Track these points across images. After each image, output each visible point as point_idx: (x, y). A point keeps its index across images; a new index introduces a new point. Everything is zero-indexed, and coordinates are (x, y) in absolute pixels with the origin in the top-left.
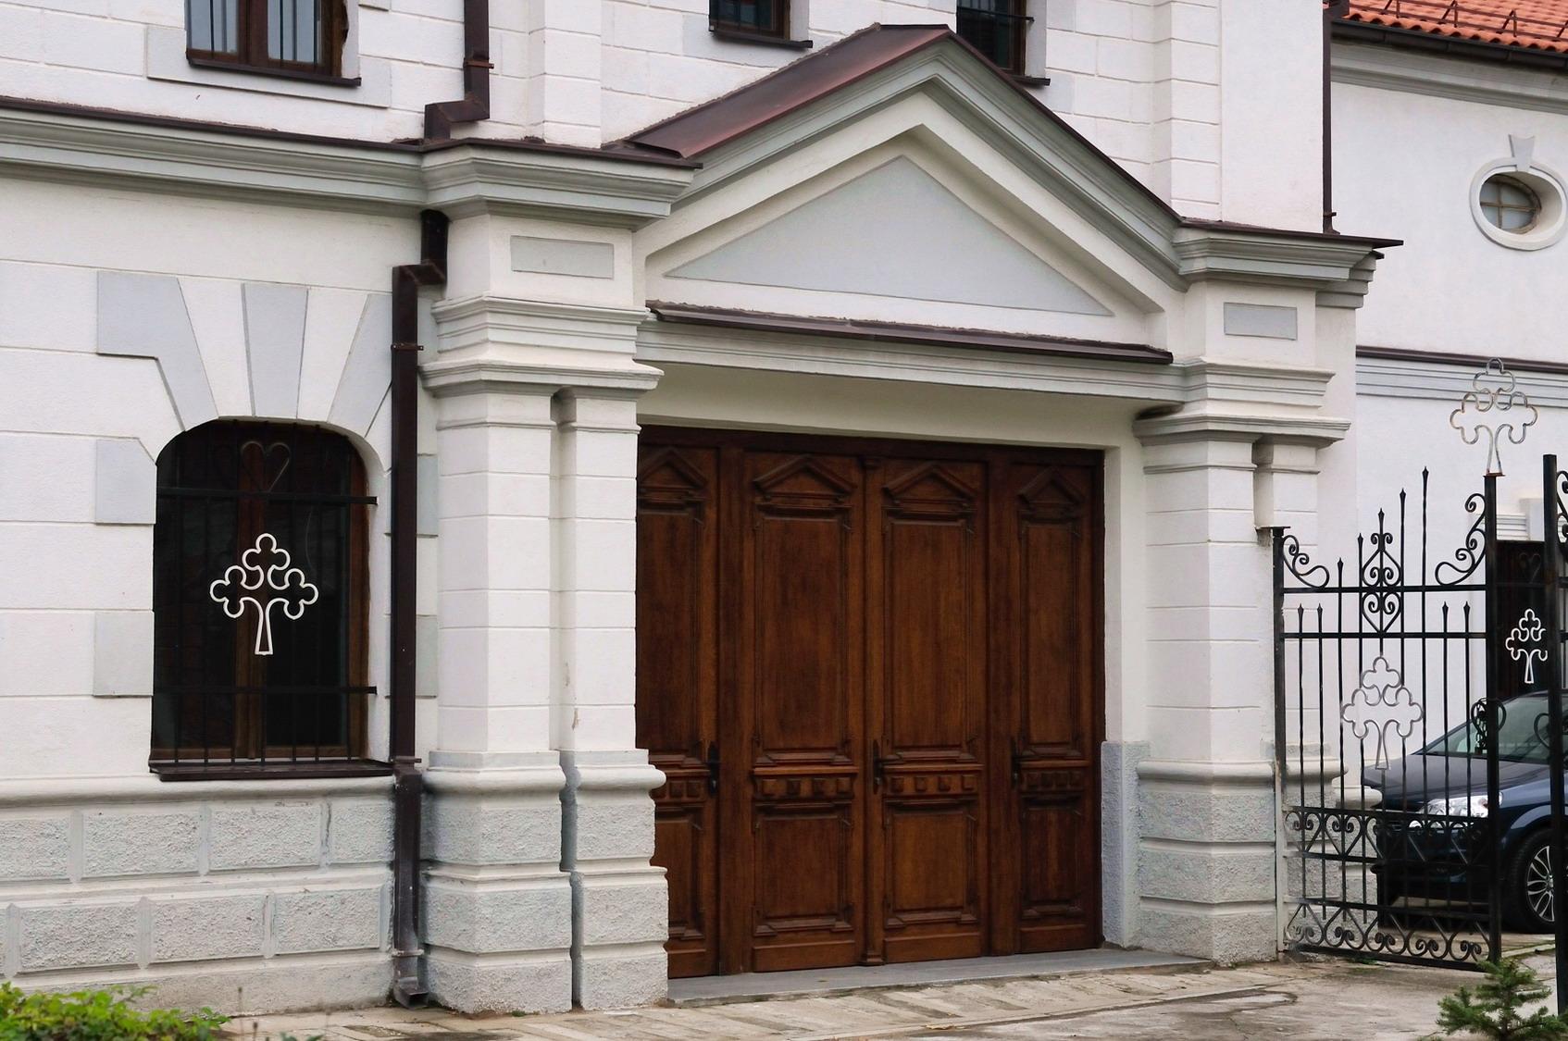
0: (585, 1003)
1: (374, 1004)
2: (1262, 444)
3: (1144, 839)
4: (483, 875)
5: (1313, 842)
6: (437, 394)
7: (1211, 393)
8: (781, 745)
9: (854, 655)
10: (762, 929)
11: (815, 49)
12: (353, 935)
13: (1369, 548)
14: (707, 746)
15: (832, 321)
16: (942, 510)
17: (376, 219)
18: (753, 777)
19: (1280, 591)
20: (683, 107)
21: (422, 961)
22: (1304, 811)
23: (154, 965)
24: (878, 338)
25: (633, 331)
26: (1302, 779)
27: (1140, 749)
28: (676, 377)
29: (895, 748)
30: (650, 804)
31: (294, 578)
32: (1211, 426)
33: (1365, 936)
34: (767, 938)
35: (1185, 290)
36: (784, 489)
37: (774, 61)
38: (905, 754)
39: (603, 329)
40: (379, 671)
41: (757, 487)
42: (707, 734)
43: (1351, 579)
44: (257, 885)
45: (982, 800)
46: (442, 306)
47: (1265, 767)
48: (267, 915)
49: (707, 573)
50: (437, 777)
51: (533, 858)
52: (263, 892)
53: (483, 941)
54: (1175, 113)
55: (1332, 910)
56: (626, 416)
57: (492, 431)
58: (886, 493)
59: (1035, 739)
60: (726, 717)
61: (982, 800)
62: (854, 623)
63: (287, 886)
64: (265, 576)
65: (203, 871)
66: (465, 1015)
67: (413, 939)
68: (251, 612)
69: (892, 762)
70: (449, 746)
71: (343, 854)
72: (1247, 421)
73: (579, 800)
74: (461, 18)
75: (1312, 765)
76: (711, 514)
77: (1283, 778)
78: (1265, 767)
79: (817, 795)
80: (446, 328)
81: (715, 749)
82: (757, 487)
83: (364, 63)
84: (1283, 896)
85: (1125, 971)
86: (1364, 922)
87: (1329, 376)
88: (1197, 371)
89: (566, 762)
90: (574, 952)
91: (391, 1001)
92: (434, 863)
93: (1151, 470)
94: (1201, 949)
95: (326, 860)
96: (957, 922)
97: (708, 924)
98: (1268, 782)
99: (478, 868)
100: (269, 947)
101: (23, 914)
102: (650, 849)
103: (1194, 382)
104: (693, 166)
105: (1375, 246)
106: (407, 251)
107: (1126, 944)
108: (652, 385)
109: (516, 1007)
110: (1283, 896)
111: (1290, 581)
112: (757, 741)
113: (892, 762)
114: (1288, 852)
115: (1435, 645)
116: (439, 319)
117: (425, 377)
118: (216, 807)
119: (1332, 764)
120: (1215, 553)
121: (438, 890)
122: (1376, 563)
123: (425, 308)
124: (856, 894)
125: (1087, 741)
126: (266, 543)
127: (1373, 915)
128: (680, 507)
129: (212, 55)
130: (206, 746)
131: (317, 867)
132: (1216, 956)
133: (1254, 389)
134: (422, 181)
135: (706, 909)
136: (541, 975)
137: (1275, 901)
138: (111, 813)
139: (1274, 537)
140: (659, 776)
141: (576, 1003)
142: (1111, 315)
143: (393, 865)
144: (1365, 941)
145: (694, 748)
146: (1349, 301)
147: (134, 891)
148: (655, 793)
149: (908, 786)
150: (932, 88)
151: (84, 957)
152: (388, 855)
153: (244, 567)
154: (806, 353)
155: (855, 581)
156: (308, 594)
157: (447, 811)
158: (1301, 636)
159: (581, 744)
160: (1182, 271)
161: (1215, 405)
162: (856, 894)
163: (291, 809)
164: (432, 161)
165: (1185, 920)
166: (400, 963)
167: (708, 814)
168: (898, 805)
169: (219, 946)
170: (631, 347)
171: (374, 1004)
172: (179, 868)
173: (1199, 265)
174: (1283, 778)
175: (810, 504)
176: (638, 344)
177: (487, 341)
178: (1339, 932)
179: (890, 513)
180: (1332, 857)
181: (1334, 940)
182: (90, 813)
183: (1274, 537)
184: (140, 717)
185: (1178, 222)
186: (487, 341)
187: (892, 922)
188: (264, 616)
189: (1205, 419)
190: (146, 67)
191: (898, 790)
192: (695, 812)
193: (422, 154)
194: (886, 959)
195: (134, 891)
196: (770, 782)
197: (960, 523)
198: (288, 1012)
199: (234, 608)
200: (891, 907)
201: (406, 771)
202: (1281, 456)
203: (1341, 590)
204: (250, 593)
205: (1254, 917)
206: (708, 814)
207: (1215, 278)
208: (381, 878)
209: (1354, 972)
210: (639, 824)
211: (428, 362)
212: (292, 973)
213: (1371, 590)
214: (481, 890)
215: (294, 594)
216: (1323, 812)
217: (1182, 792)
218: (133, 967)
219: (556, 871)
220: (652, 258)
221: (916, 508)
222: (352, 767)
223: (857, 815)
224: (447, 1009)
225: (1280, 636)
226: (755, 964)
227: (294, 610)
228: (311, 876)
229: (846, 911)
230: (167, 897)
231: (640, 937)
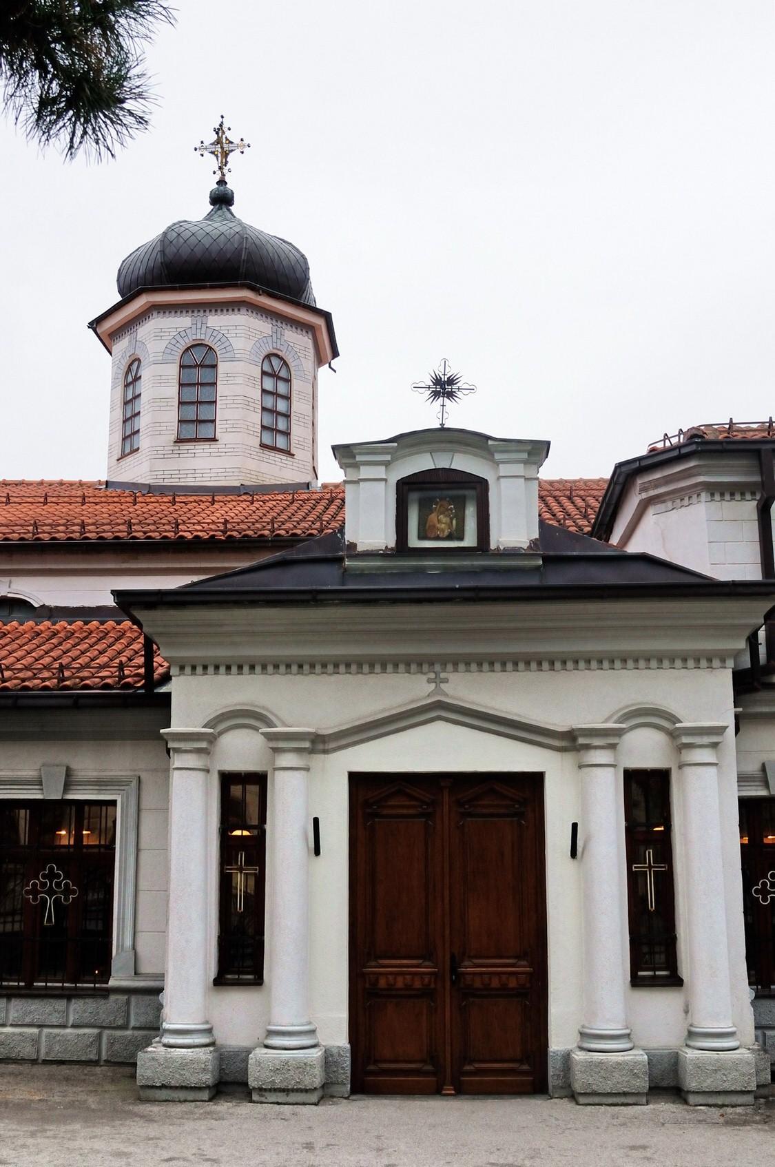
215: (67, 891)
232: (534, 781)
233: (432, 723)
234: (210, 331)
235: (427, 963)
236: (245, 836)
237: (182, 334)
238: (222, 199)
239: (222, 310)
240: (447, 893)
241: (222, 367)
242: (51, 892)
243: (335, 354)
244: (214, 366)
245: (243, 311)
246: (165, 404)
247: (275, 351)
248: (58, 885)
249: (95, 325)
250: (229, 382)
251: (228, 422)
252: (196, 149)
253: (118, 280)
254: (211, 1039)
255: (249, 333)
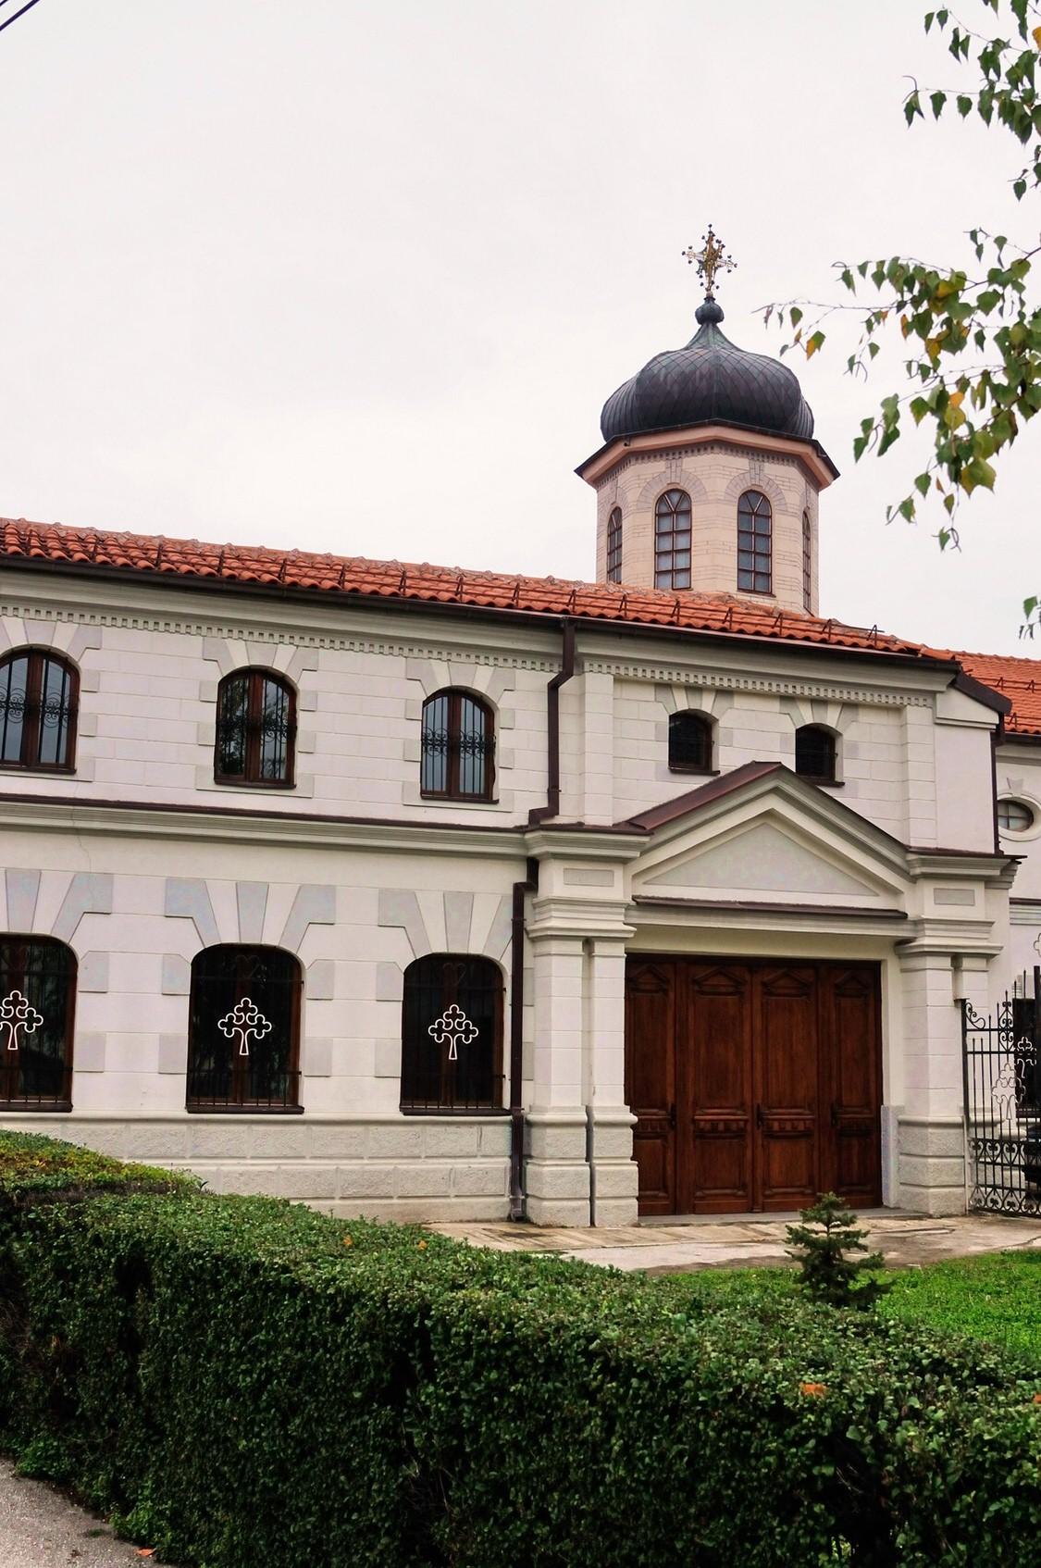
0: (596, 1224)
1: (501, 1220)
2: (957, 958)
3: (901, 1154)
4: (548, 1162)
5: (981, 1156)
6: (534, 940)
7: (927, 933)
8: (709, 1105)
9: (747, 1065)
10: (699, 1194)
11: (722, 774)
12: (492, 1188)
13: (1002, 1009)
14: (670, 1105)
15: (729, 902)
16: (793, 992)
17: (507, 862)
18: (694, 1121)
19: (965, 1031)
20: (657, 804)
21: (524, 1202)
22: (976, 1140)
23: (400, 1197)
24: (749, 910)
25: (623, 910)
26: (976, 1125)
27: (900, 1109)
28: (642, 930)
29: (769, 1108)
30: (631, 1131)
31: (260, 1019)
32: (926, 949)
33: (1021, 1204)
34: (702, 1198)
35: (915, 883)
36: (710, 982)
37: (705, 780)
38: (775, 1111)
39: (957, 927)
40: (507, 1070)
41: (695, 982)
42: (670, 1099)
43: (995, 1026)
44: (446, 1163)
45: (816, 1134)
46: (535, 900)
47: (958, 1118)
48: (452, 1178)
49: (670, 1022)
50: (532, 1117)
51: (572, 1156)
52: (450, 1167)
53: (546, 1192)
54: (911, 796)
55: (989, 1190)
56: (620, 949)
57: (554, 957)
58: (764, 984)
59: (844, 1103)
60: (680, 1091)
61: (816, 1134)
62: (747, 1046)
63: (461, 1165)
64: (454, 1024)
65: (423, 1156)
66: (539, 1227)
67: (519, 1191)
68: (238, 1035)
69: (768, 1114)
70: (538, 1103)
71: (488, 1152)
72: (946, 946)
73: (595, 1129)
74: (547, 769)
75: (988, 1118)
76: (672, 995)
77: (968, 1124)
78: (958, 1118)
79: (727, 1129)
80: (537, 910)
81: (674, 1107)
82: (695, 982)
83: (501, 792)
84: (968, 1183)
85: (880, 1218)
86: (1018, 1197)
87: (993, 923)
88: (919, 923)
89: (588, 1111)
90: (592, 1199)
91: (509, 1219)
92: (530, 1157)
93: (904, 971)
94: (924, 1210)
95: (480, 1154)
96: (803, 1194)
97: (671, 1190)
98: (960, 1126)
99: (545, 1159)
100: (452, 1192)
101: (342, 1172)
102: (631, 1153)
103: (920, 927)
104: (650, 833)
105: (1015, 860)
106: (520, 876)
107: (892, 1206)
108: (632, 935)
109: (562, 1224)
110: (968, 1183)
111: (969, 1026)
112: (695, 1104)
113: (768, 1114)
114: (970, 1161)
115: (986, 1057)
116: (535, 906)
117: (528, 933)
118: (428, 1128)
119: (996, 1117)
120: (931, 1012)
121: (530, 1169)
122: (1005, 1017)
123: (528, 902)
124: (748, 1178)
125: (873, 1107)
126: (454, 1009)
127: (1023, 1194)
128: (656, 992)
129: (433, 792)
130: (214, 1096)
131: (475, 1157)
132: (931, 1212)
133: (969, 931)
134: (524, 844)
135: (670, 1183)
136: (574, 1210)
137: (964, 1186)
138: (382, 1129)
139: (961, 1003)
140: (634, 1119)
141: (592, 1223)
142: (877, 895)
143: (511, 1157)
144: (1020, 1208)
145: (663, 1106)
146: (1005, 886)
147: (391, 1164)
148: (633, 1127)
149: (776, 1126)
150: (776, 791)
151: (368, 1192)
152: (509, 1153)
153: (444, 1020)
154: (713, 918)
155: (747, 1028)
156: (38, 1020)
157: (535, 1132)
158: (974, 1053)
159: (596, 1103)
160: (911, 873)
161: (928, 939)
162: (748, 1178)
163: (464, 1130)
164: (528, 836)
165: (918, 1194)
166: (514, 1201)
167: (670, 1136)
168: (770, 1135)
169: (429, 1190)
170: (622, 918)
171: (501, 1220)
172: (411, 1154)
173: (918, 871)
174: (968, 1124)
175: (723, 990)
176: (626, 916)
177: (551, 917)
178: (1009, 1204)
179: (765, 993)
180: (989, 1163)
181: (990, 1205)
182: (372, 1128)
183: (961, 1003)
184: (396, 1086)
185: (905, 849)
186: (551, 917)
187: (767, 1192)
188: (453, 1042)
189: (923, 946)
190: (403, 799)
191: (770, 1128)
192: (664, 1137)
193: (524, 833)
194: (763, 1210)
195: (391, 1164)
196: (702, 1123)
197: (804, 997)
198: (461, 1221)
199: (439, 1038)
200: (766, 1185)
201: (516, 1114)
202: (966, 963)
203: (990, 1030)
204: (22, 1020)
205: (954, 1194)
206: (670, 1136)
207: (926, 876)
208: (505, 1162)
209: (1003, 1221)
210: (625, 1139)
211: (529, 926)
212: (463, 1204)
213: (1003, 1030)
214: (546, 1169)
215: (467, 1032)
216: (985, 1141)
217: (916, 1130)
218: (391, 1197)
219: (584, 1162)
220: (635, 876)
221: (780, 991)
222: (494, 1112)
223: (749, 1141)
224: (532, 1223)
225: (965, 1053)
226: (694, 1210)
227: (259, 1034)
228: (472, 1160)
229: (743, 1186)
230: (405, 1167)
231: (624, 1194)
235: (739, 1112)
238: (709, 316)
239: (693, 451)
240: (758, 1057)
241: (697, 511)
242: (245, 1026)
243: (835, 474)
244: (688, 512)
245: (716, 450)
247: (754, 488)
249: (580, 471)
253: (602, 428)
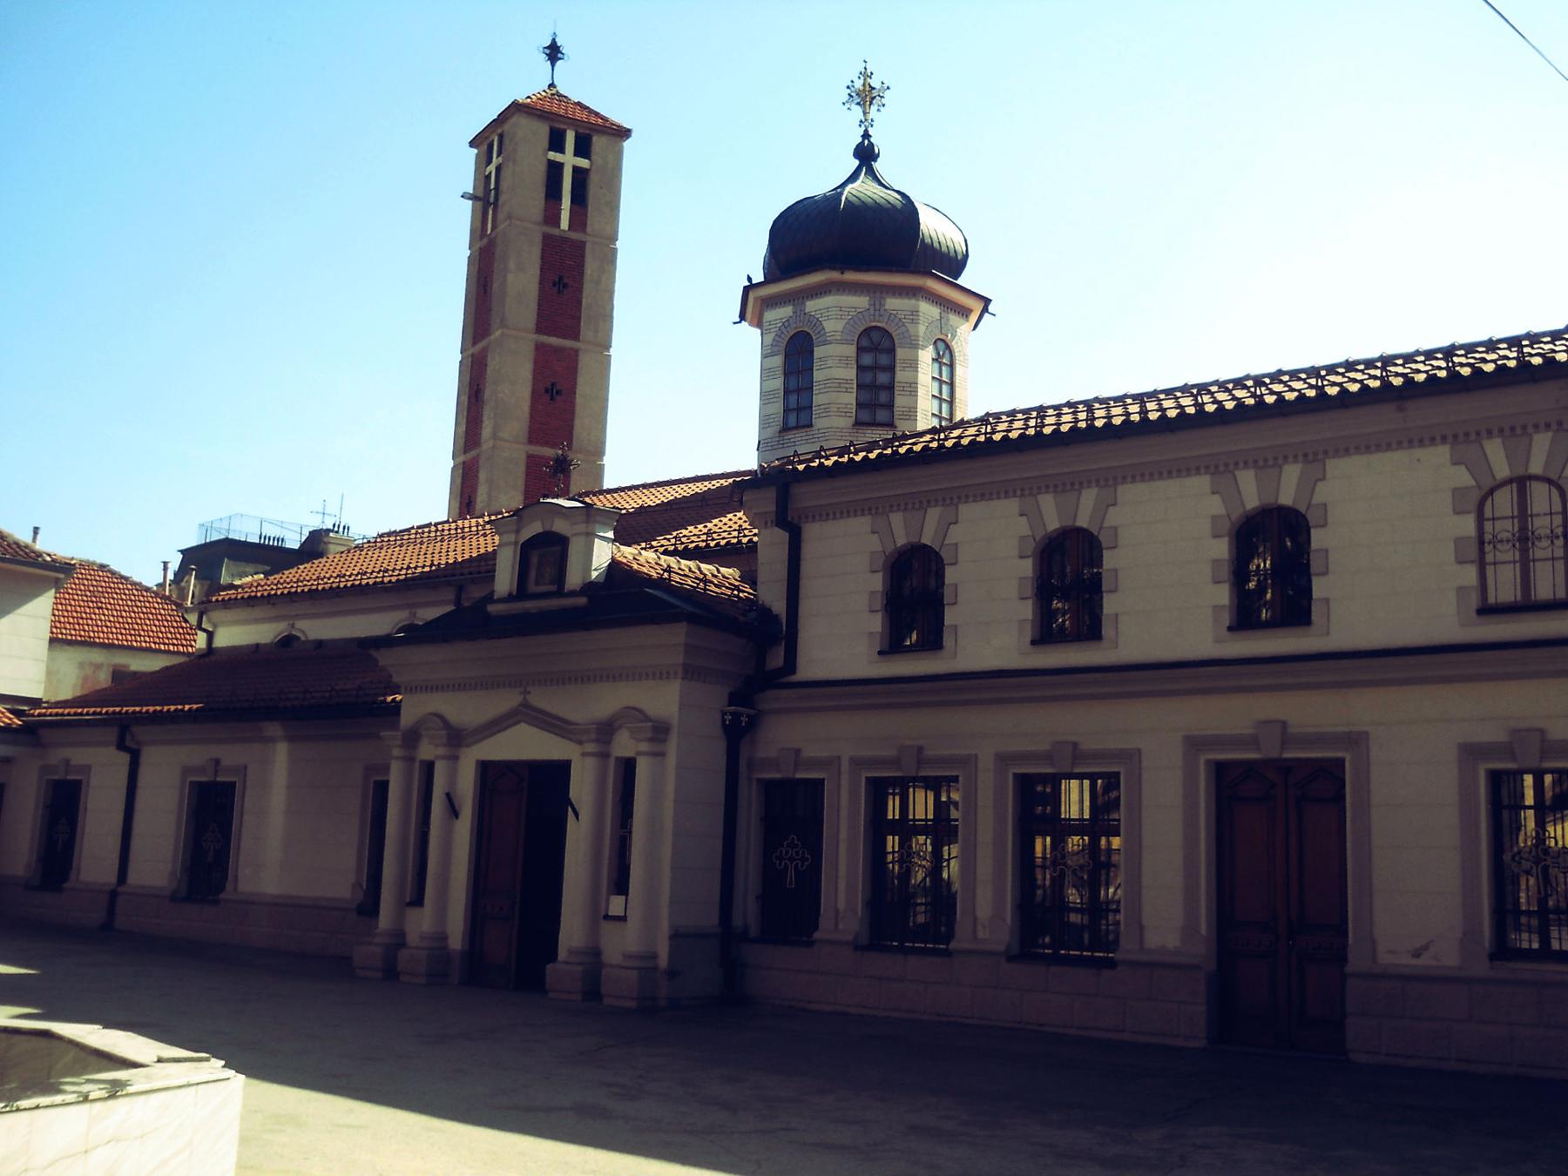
215: (803, 859)
232: (1340, 763)
233: (954, 671)
234: (807, 317)
236: (234, 653)
237: (786, 324)
238: (866, 154)
246: (772, 396)
248: (797, 853)
249: (742, 317)
250: (822, 367)
251: (821, 407)
252: (844, 104)
254: (105, 668)
255: (841, 313)
